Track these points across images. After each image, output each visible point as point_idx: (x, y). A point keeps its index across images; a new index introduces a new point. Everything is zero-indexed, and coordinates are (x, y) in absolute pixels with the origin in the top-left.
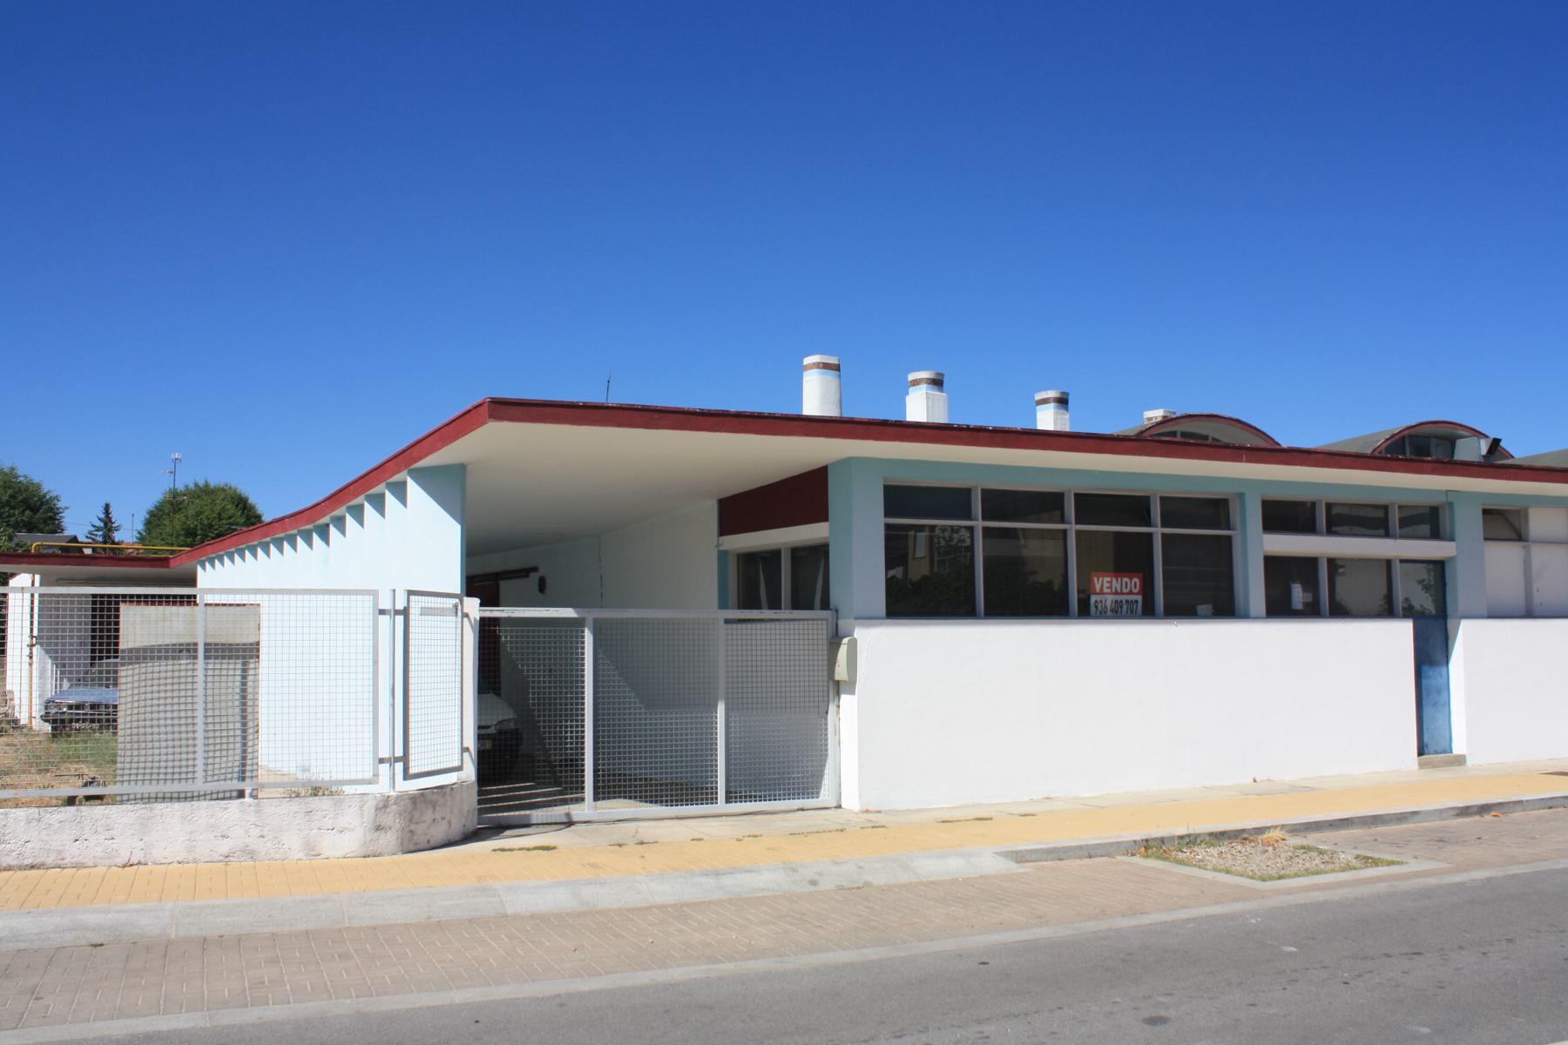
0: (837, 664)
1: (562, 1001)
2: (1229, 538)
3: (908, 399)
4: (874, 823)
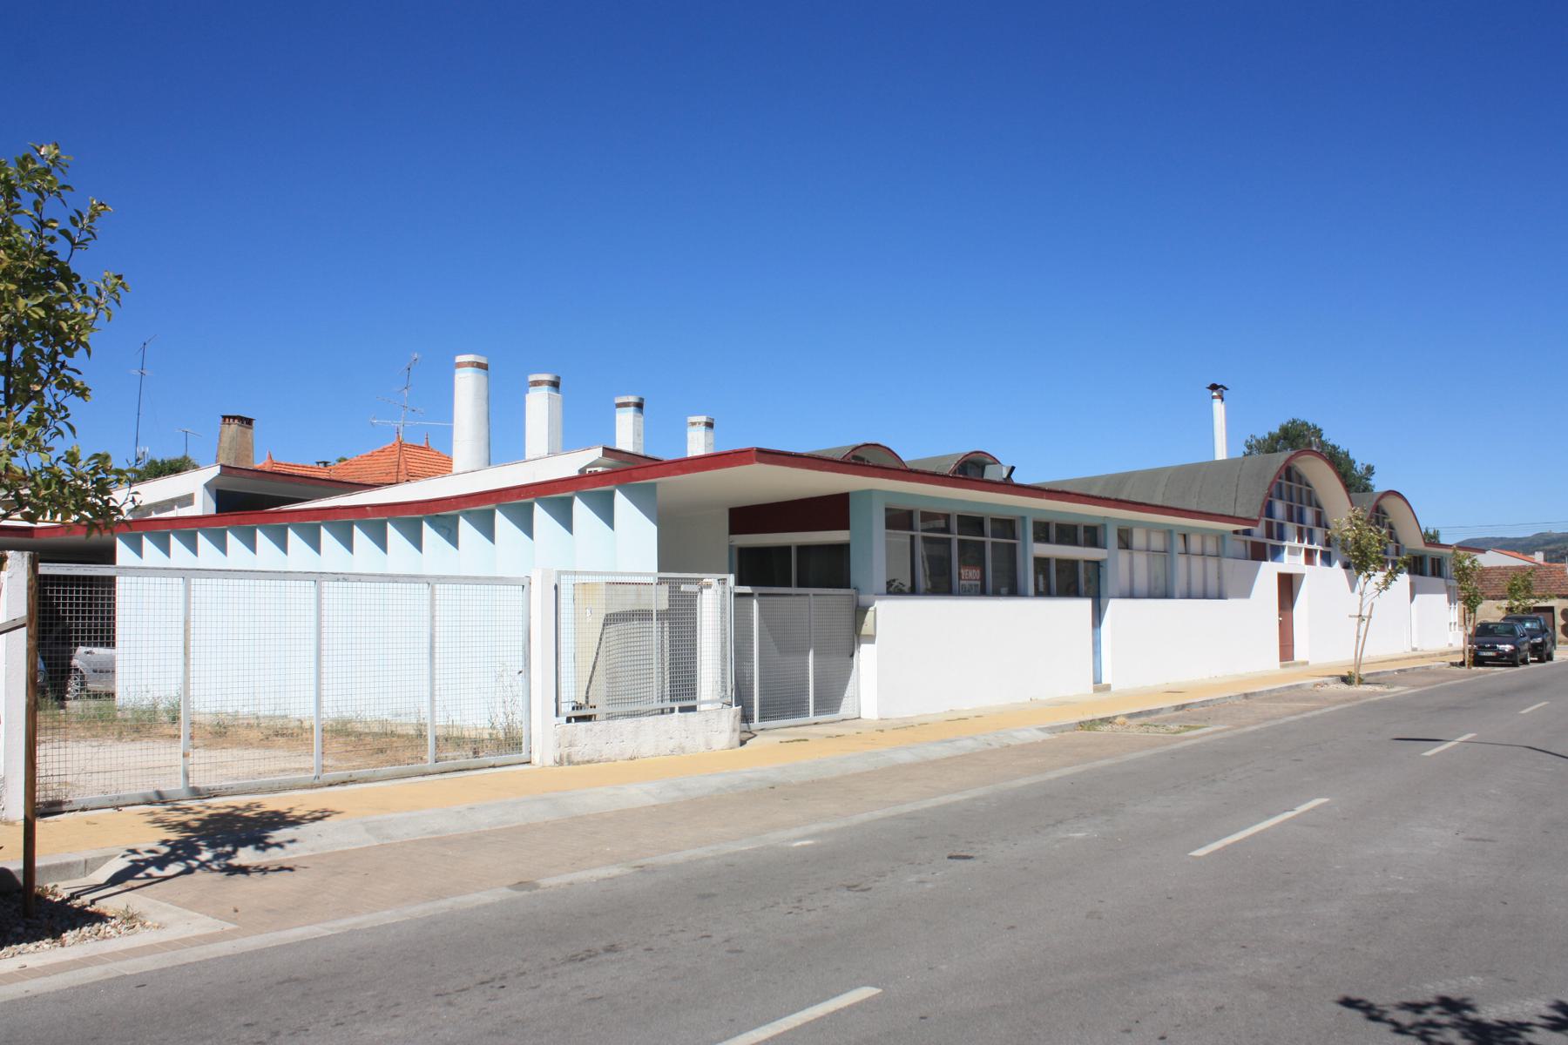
1: (910, 817)
2: (1015, 545)
3: (527, 396)
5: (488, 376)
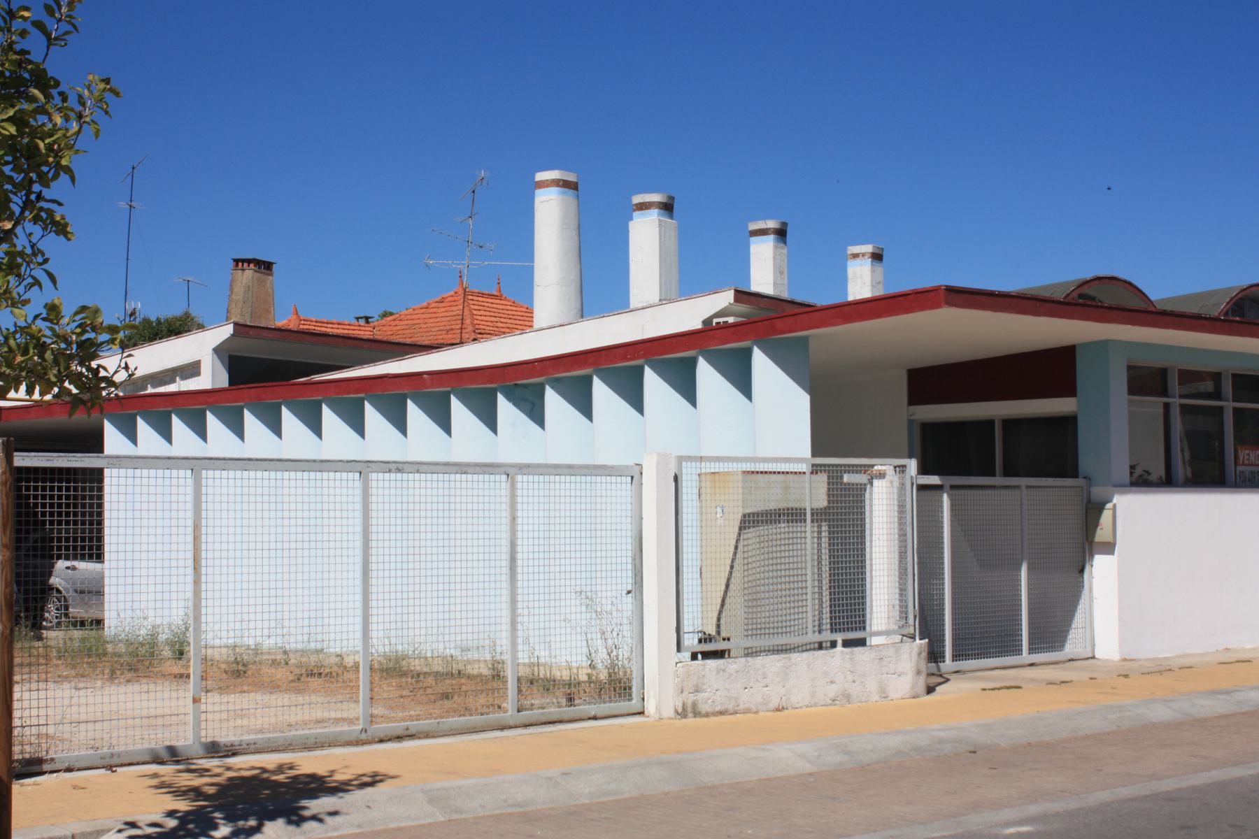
0: (1099, 527)
3: (631, 224)
4: (1125, 671)
5: (578, 197)
